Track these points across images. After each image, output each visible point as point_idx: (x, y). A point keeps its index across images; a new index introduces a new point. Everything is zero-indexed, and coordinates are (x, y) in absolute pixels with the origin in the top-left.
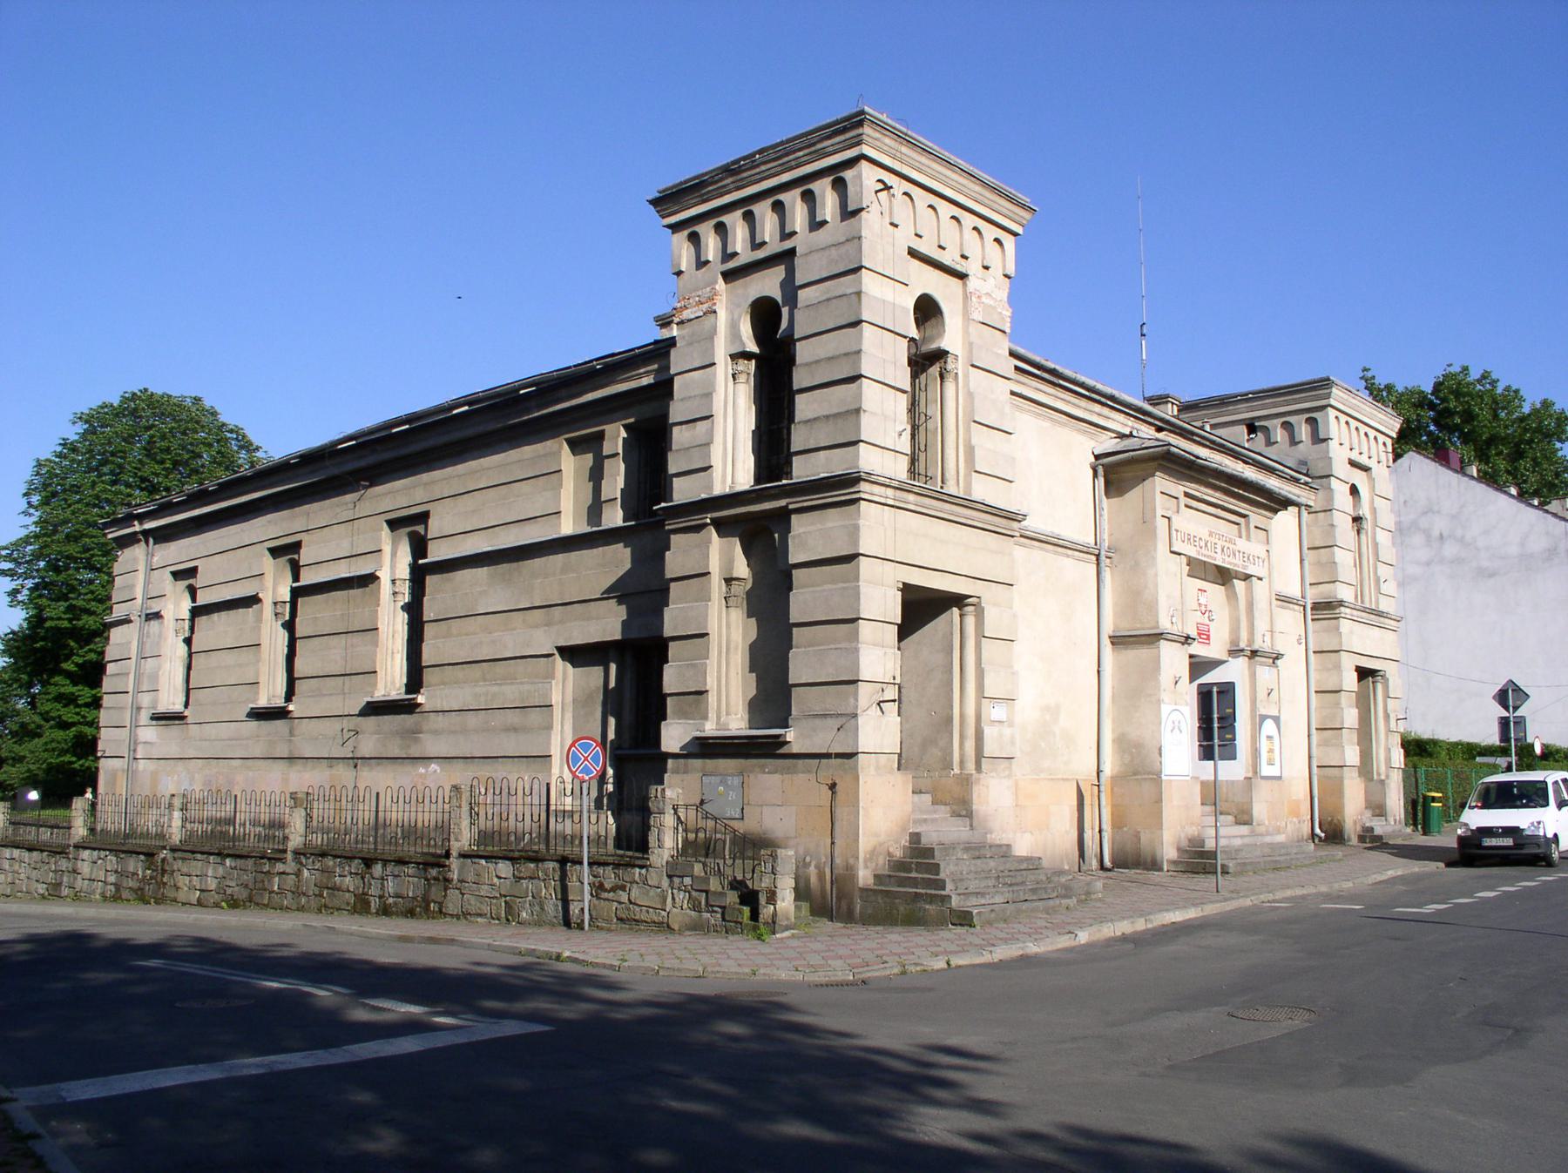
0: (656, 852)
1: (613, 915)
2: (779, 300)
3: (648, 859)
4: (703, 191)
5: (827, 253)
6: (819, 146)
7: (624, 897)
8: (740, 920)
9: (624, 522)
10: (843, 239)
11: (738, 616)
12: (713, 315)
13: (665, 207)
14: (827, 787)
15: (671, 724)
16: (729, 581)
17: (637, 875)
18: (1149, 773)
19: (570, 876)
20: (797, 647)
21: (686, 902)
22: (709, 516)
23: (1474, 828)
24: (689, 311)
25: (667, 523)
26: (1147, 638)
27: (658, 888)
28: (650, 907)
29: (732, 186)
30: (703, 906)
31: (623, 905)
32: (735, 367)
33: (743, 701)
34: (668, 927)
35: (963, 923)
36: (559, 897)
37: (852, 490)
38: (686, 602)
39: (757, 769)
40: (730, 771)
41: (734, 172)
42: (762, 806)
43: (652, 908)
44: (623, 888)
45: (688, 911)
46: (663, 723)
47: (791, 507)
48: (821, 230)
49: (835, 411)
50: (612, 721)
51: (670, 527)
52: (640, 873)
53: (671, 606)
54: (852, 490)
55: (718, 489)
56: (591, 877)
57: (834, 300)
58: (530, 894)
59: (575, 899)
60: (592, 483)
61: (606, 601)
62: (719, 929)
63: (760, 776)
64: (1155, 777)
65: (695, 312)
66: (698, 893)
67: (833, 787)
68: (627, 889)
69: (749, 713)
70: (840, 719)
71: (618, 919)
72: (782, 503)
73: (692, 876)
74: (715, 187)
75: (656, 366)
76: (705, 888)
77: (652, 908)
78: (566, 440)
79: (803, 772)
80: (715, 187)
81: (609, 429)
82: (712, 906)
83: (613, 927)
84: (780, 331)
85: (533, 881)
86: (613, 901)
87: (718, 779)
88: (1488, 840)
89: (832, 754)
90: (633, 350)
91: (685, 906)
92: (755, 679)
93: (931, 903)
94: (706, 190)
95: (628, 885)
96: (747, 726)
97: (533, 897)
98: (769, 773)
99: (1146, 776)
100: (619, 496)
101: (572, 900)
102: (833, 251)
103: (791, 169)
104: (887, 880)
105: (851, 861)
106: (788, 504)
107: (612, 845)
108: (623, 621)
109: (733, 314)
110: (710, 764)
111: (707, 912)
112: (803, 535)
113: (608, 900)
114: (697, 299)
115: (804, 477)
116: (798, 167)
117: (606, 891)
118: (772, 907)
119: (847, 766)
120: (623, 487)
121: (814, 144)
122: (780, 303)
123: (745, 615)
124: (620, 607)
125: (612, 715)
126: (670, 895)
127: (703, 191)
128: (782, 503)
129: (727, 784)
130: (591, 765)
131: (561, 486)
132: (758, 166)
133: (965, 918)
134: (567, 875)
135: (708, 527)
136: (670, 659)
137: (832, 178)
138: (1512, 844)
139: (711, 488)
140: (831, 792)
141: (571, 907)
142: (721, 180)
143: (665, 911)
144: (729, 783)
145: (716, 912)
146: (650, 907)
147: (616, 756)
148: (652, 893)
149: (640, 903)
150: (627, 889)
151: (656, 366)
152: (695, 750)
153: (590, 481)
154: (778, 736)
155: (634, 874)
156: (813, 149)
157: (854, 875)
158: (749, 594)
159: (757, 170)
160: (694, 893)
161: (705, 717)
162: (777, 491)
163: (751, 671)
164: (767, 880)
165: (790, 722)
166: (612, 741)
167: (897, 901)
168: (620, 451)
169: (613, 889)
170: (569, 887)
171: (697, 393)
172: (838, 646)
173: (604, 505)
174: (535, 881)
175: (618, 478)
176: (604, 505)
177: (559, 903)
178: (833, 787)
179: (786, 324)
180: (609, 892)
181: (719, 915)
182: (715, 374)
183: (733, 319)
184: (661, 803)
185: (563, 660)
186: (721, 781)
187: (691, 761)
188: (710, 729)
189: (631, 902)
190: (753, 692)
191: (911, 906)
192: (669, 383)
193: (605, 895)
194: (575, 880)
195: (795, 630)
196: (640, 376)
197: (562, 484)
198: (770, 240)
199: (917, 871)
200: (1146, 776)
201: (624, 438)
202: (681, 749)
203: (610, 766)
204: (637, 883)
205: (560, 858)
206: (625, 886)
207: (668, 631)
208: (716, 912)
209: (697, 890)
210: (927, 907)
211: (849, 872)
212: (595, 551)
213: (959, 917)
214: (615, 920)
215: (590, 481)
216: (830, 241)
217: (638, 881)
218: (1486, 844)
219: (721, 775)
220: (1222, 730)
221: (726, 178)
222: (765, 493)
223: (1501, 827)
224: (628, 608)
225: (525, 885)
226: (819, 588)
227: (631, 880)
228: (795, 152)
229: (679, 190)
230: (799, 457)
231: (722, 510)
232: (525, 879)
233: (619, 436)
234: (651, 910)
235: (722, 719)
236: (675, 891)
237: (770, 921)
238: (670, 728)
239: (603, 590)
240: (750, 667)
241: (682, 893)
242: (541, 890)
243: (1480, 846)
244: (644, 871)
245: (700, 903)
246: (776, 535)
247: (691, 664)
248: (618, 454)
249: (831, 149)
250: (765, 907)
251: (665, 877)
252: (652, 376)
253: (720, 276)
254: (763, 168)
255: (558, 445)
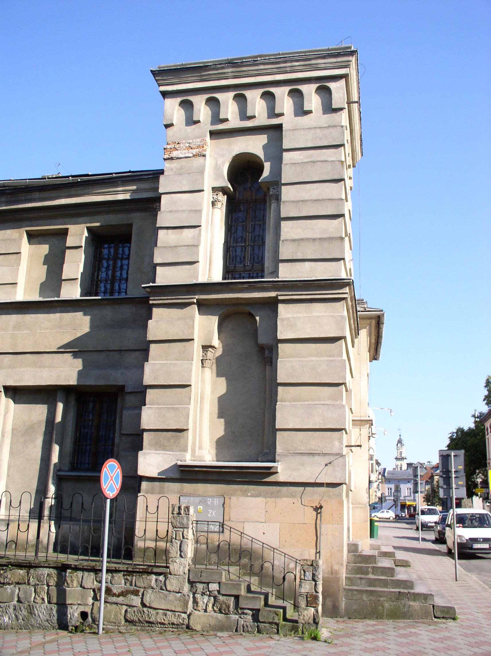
0: (177, 561)
1: (122, 618)
2: (262, 157)
3: (168, 567)
4: (204, 74)
5: (313, 131)
6: (313, 62)
7: (136, 601)
8: (276, 621)
9: (81, 296)
10: (326, 125)
11: (209, 374)
12: (204, 158)
13: (165, 78)
14: (312, 509)
15: (148, 453)
16: (205, 348)
17: (153, 581)
18: (360, 504)
19: (69, 582)
20: (282, 401)
21: (210, 605)
22: (197, 297)
23: (468, 538)
24: (179, 152)
25: (151, 298)
26: (359, 422)
27: (179, 592)
28: (168, 610)
29: (230, 75)
30: (232, 608)
31: (135, 609)
32: (215, 197)
33: (211, 440)
34: (188, 627)
35: (447, 616)
36: (55, 600)
37: (340, 291)
38: (167, 360)
39: (239, 493)
40: (210, 494)
41: (235, 65)
42: (244, 522)
43: (171, 611)
44: (135, 593)
45: (213, 613)
46: (140, 452)
47: (280, 298)
48: (305, 117)
49: (318, 236)
50: (56, 449)
51: (154, 302)
52: (156, 580)
53: (149, 362)
54: (340, 291)
55: (202, 279)
56: (95, 583)
57: (319, 163)
58: (16, 599)
59: (75, 603)
60: (46, 267)
61: (61, 355)
62: (250, 629)
63: (242, 499)
64: (364, 506)
65: (185, 153)
66: (225, 598)
67: (318, 509)
68: (140, 594)
69: (217, 449)
70: (328, 457)
71: (126, 620)
72: (273, 294)
73: (219, 583)
74: (216, 72)
75: (134, 187)
76: (234, 593)
77: (171, 611)
78: (27, 231)
79: (287, 497)
80: (216, 72)
81: (73, 229)
82: (241, 609)
83: (122, 629)
84: (261, 178)
85: (20, 586)
86: (122, 605)
87: (197, 499)
88: (476, 545)
89: (324, 483)
90: (112, 174)
91: (210, 608)
92: (223, 423)
93: (414, 600)
94: (207, 73)
95: (142, 590)
96: (215, 459)
97: (19, 601)
98: (252, 496)
99: (357, 506)
100: (79, 277)
101: (71, 604)
102: (318, 131)
103: (286, 72)
104: (359, 581)
105: (336, 567)
106: (277, 295)
107: (52, 549)
108: (79, 371)
109: (217, 162)
110: (188, 487)
111: (236, 614)
112: (291, 319)
113: (117, 604)
114: (188, 145)
115: (306, 278)
116: (290, 73)
117: (114, 595)
118: (313, 609)
119: (331, 494)
120: (82, 272)
121: (310, 60)
122: (263, 160)
123: (215, 374)
124: (75, 360)
125: (56, 443)
126: (191, 599)
127: (204, 74)
128: (273, 294)
129: (207, 504)
130: (114, 484)
131: (19, 264)
132: (257, 65)
133: (448, 612)
134: (66, 580)
135: (193, 306)
136: (147, 402)
137: (318, 85)
138: (488, 547)
139: (197, 277)
140: (316, 513)
141: (70, 610)
142: (223, 68)
143: (185, 613)
144: (209, 503)
145: (246, 614)
146: (168, 610)
147: (57, 476)
148: (171, 597)
149: (155, 607)
150: (140, 594)
151: (134, 187)
152: (176, 475)
153: (44, 264)
154: (269, 468)
155: (150, 580)
156: (308, 62)
157: (339, 578)
158: (218, 360)
159: (256, 68)
160: (221, 598)
161: (185, 450)
162: (270, 285)
163: (220, 416)
164: (307, 586)
165: (277, 458)
166: (55, 464)
167: (382, 599)
168: (83, 245)
169: (123, 594)
170: (67, 592)
171: (184, 208)
172: (325, 402)
173: (63, 282)
174: (22, 587)
175: (80, 264)
176: (63, 282)
177: (55, 608)
178: (318, 509)
179: (268, 174)
180: (119, 596)
181: (250, 617)
182: (203, 198)
183: (216, 164)
184: (185, 519)
185: (6, 396)
186: (200, 501)
187: (167, 484)
188: (189, 460)
189: (144, 605)
190: (220, 431)
191: (395, 603)
192: (158, 199)
193: (114, 599)
194: (75, 585)
195: (280, 389)
196: (116, 193)
197: (20, 263)
198: (259, 116)
199: (373, 573)
200: (357, 506)
201: (86, 236)
202: (159, 474)
203: (53, 483)
204: (153, 588)
205: (60, 565)
206: (138, 591)
207: (147, 380)
208: (246, 614)
209: (223, 595)
210: (411, 603)
211: (334, 576)
212: (52, 316)
213: (442, 612)
214: (123, 622)
215: (44, 264)
216: (313, 124)
217: (155, 586)
218: (475, 547)
219: (200, 496)
220: (457, 479)
221: (228, 67)
222: (232, 286)
223: (482, 538)
224: (83, 361)
225: (9, 591)
226: (305, 359)
227: (146, 585)
228: (292, 61)
229: (183, 68)
230: (285, 264)
231: (211, 294)
232: (9, 584)
233: (84, 234)
234: (169, 613)
235: (197, 452)
236: (198, 596)
237: (311, 621)
238: (147, 457)
239: (60, 346)
240: (219, 414)
241: (206, 598)
242: (31, 595)
243: (471, 548)
244: (161, 578)
245: (228, 607)
246: (258, 318)
247: (173, 408)
248: (82, 247)
249: (323, 66)
250: (305, 609)
251: (187, 583)
252: (130, 194)
253: (208, 133)
254: (262, 67)
255: (17, 235)
